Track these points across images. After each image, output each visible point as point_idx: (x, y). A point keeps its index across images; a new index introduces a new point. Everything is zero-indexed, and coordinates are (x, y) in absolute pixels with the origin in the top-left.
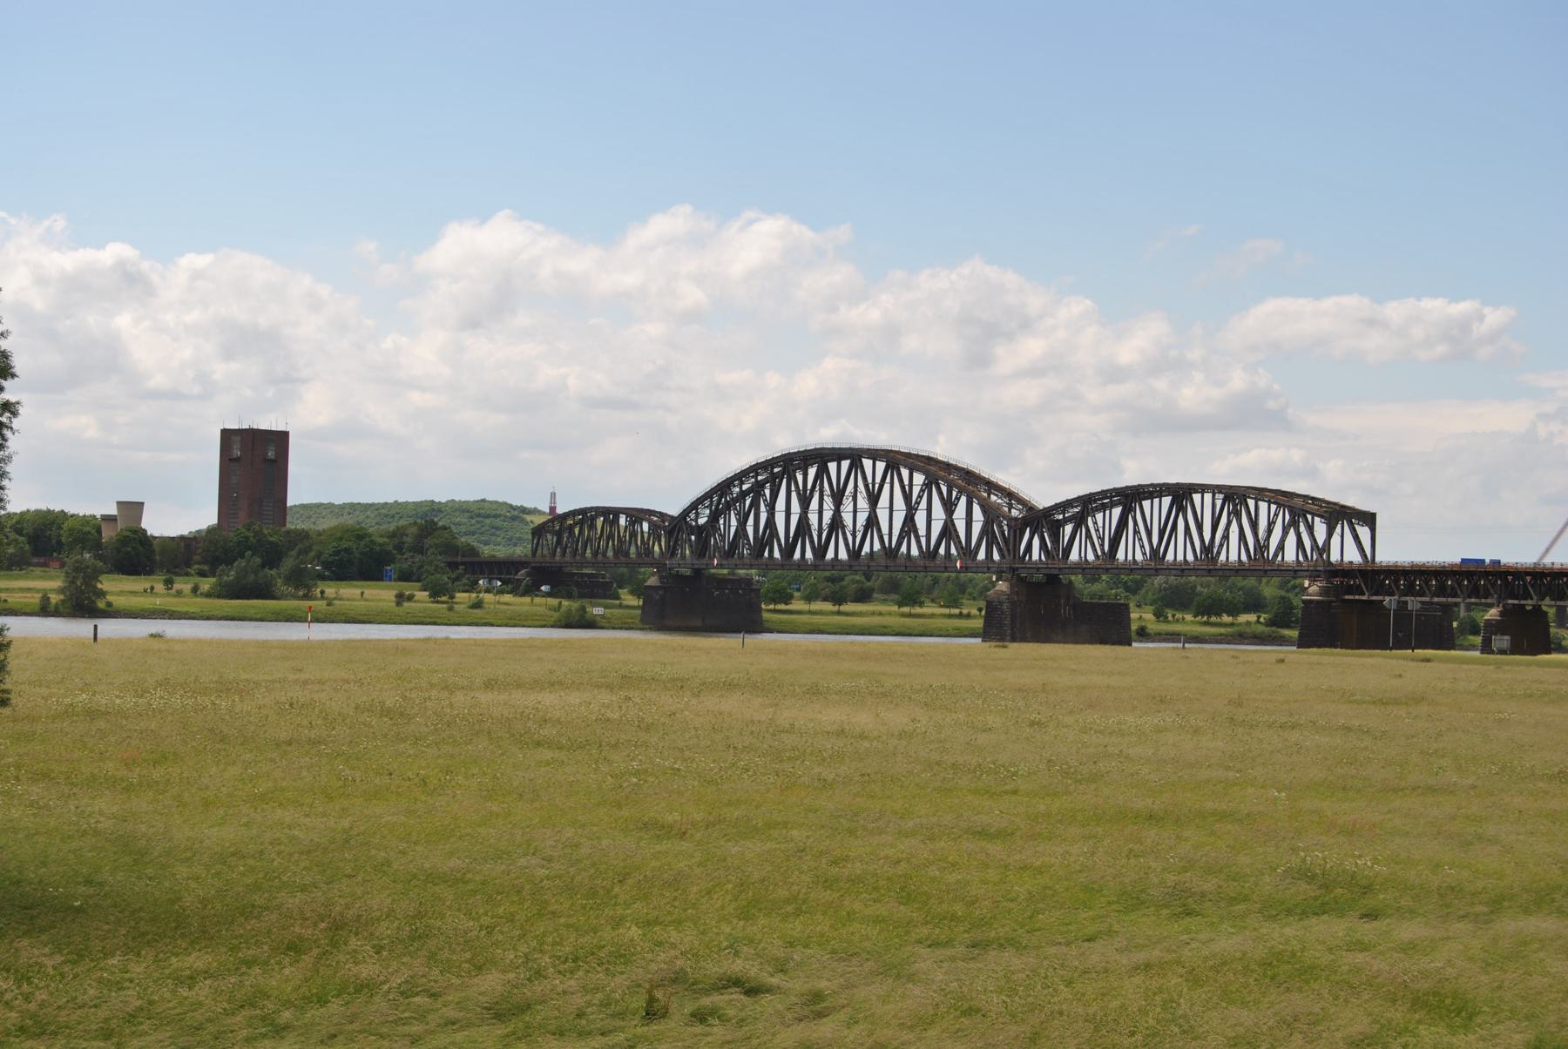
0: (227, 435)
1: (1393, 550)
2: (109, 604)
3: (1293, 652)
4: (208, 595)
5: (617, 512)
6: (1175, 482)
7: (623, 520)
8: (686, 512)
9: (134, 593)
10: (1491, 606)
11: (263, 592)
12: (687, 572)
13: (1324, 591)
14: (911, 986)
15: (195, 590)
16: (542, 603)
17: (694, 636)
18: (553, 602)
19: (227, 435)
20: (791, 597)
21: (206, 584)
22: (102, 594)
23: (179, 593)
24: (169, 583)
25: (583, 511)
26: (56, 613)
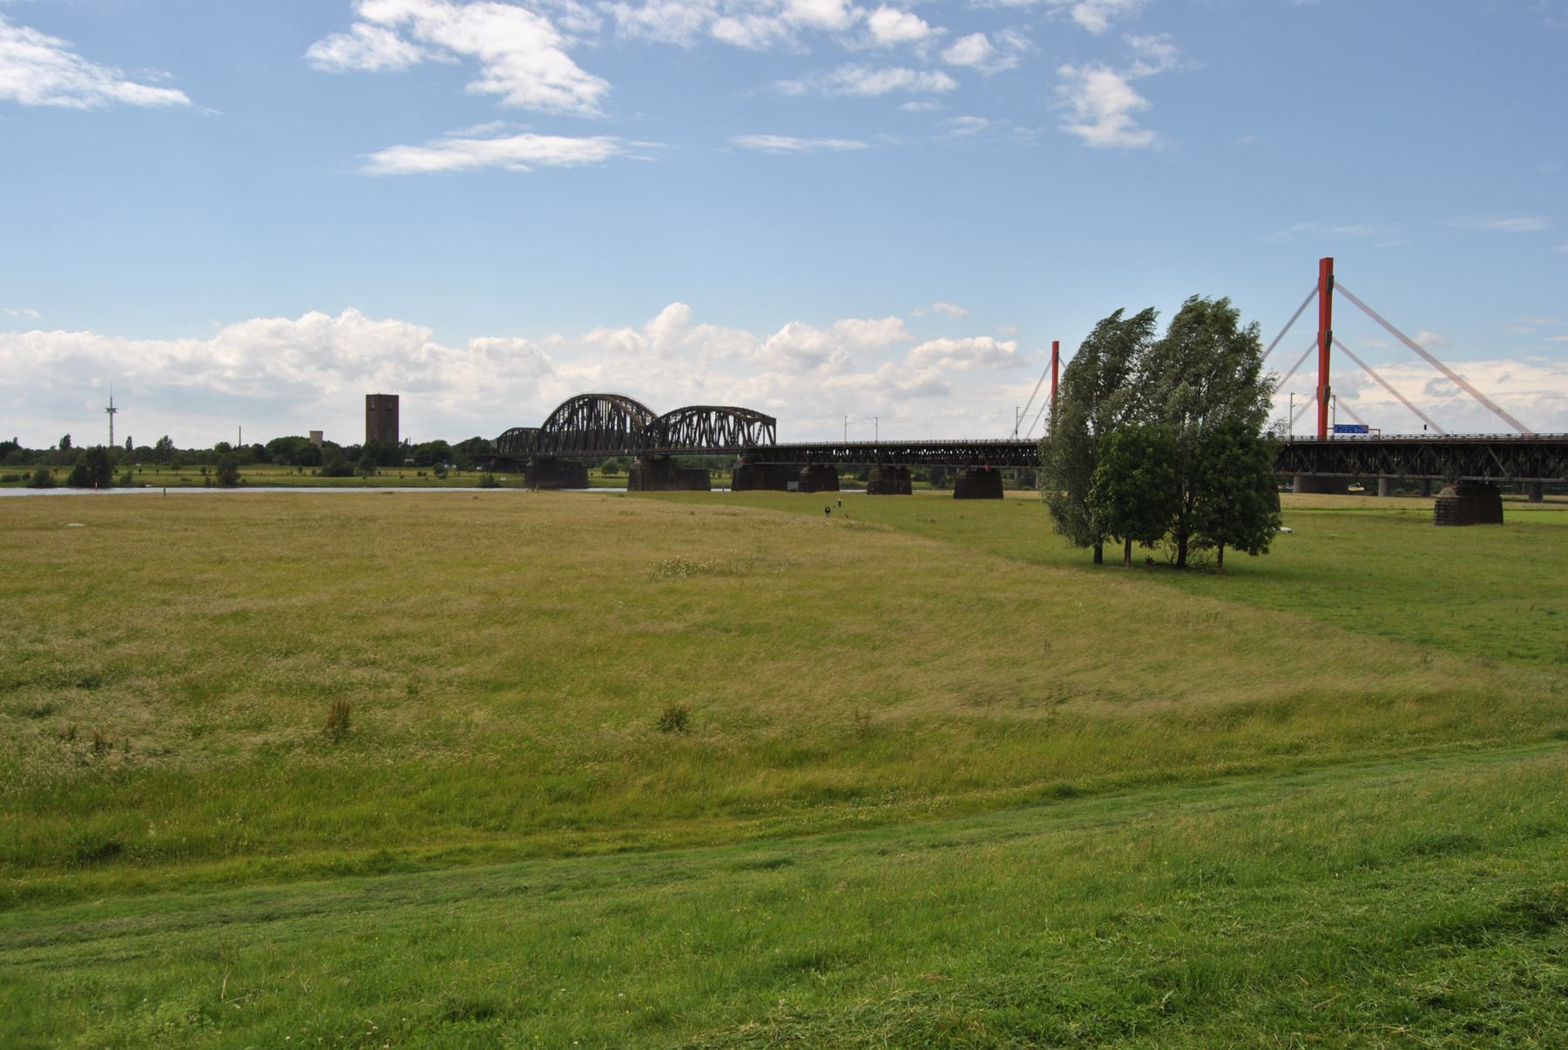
0: (369, 397)
1: (786, 436)
2: (244, 481)
3: (621, 495)
4: (320, 475)
5: (708, 410)
6: (187, 449)
7: (713, 415)
8: (667, 416)
9: (282, 475)
10: (805, 466)
11: (349, 473)
12: (657, 457)
13: (746, 460)
14: (564, 815)
15: (313, 473)
16: (478, 474)
17: (1491, 526)
18: (481, 474)
19: (369, 397)
20: (617, 470)
21: (319, 471)
22: (239, 476)
23: (304, 475)
24: (300, 470)
25: (683, 411)
26: (214, 486)
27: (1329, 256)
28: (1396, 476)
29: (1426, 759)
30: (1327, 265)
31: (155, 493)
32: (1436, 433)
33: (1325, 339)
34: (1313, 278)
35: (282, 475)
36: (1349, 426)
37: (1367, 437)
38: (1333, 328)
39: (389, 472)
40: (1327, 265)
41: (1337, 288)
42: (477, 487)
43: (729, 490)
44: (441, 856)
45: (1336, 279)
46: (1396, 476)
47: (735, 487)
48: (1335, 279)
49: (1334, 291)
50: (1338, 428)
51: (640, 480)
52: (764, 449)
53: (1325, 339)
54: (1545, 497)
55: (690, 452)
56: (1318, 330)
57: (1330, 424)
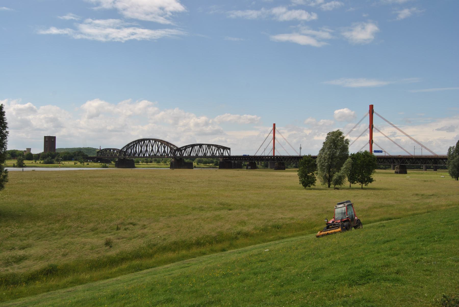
0: (45, 137)
1: (234, 153)
4: (42, 163)
11: (52, 163)
19: (45, 137)
21: (42, 162)
22: (24, 163)
27: (373, 104)
28: (442, 165)
29: (404, 243)
30: (371, 107)
31: (97, 170)
32: (409, 155)
33: (371, 127)
34: (368, 109)
35: (29, 163)
36: (378, 151)
37: (382, 154)
38: (373, 124)
39: (65, 163)
40: (371, 107)
41: (375, 113)
42: (101, 168)
43: (169, 169)
44: (410, 215)
45: (374, 111)
46: (442, 165)
47: (171, 168)
48: (374, 110)
49: (374, 114)
50: (375, 151)
51: (174, 166)
52: (226, 157)
53: (371, 127)
54: (438, 170)
55: (143, 157)
56: (369, 124)
57: (373, 150)
